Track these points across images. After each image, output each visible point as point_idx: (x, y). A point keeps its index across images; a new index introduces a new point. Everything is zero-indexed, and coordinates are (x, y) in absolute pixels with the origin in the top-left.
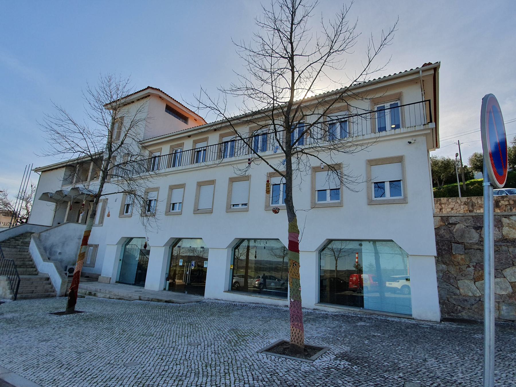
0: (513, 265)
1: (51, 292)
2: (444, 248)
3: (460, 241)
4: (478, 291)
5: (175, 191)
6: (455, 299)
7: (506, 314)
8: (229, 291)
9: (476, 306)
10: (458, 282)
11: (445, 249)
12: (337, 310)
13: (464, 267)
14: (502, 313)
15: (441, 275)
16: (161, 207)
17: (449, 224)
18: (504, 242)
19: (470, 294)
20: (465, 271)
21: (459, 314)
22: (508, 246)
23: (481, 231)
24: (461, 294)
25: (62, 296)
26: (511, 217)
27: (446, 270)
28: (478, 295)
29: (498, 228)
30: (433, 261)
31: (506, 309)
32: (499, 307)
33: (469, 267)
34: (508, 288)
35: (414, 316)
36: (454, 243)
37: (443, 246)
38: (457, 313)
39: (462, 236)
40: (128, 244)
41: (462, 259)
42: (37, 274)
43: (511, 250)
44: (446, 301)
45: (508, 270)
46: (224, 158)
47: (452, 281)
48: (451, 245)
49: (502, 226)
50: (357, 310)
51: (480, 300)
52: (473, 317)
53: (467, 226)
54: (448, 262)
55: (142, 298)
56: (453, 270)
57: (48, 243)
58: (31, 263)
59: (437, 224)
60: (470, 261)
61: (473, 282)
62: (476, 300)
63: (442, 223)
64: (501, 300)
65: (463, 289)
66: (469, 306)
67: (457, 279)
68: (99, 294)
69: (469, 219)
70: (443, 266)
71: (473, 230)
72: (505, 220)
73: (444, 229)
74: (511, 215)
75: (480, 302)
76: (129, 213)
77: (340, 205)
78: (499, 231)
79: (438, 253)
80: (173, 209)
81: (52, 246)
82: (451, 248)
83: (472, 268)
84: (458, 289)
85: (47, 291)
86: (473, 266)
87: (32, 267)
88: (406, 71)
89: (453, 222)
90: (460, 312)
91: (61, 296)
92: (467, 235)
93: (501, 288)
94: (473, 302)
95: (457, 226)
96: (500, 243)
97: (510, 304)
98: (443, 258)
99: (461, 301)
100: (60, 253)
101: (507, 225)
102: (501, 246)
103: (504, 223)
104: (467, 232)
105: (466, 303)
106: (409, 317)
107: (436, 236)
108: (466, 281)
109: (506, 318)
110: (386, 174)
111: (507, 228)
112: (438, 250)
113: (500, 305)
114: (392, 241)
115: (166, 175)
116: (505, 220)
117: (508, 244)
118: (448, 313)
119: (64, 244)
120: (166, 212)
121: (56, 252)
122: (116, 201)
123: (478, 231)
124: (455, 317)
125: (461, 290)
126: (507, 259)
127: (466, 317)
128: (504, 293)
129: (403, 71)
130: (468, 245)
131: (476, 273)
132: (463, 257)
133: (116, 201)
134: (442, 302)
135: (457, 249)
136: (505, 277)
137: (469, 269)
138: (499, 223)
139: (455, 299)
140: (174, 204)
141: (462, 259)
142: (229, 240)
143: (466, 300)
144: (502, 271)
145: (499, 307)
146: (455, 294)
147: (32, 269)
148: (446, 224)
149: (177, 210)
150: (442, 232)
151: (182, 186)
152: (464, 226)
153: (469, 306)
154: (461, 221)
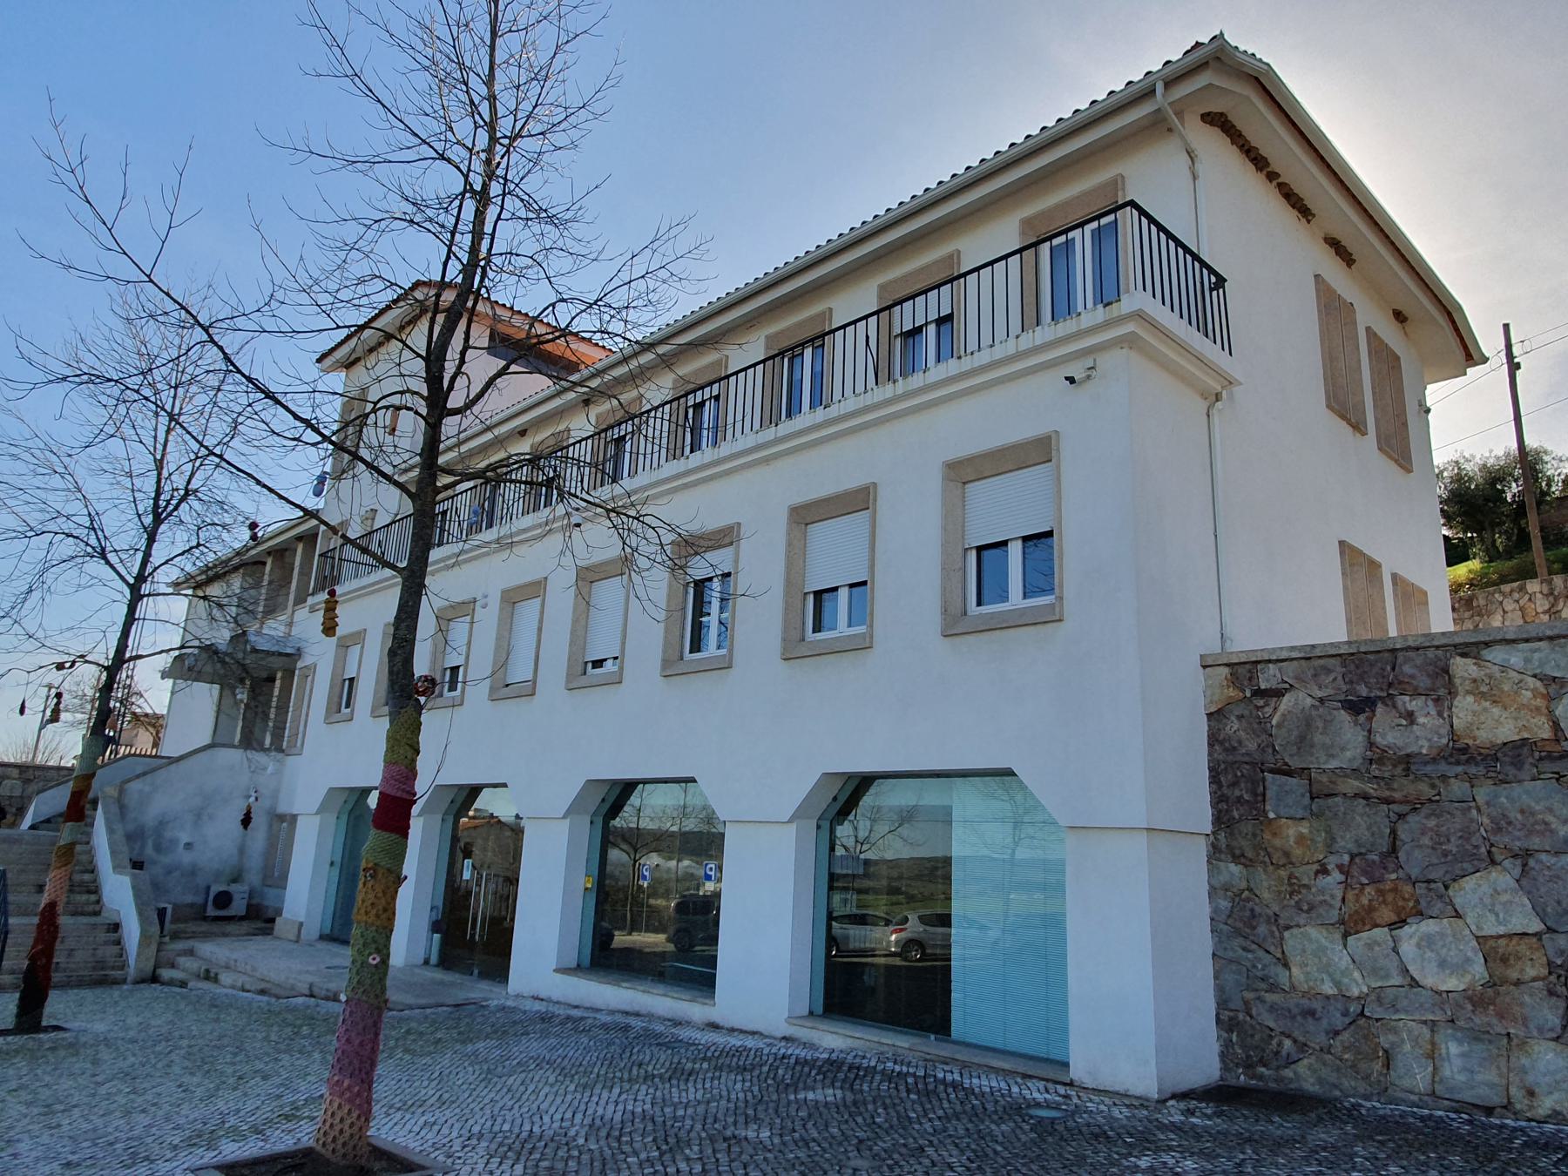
0: (1493, 862)
1: (113, 968)
2: (1237, 793)
3: (1295, 763)
4: (1356, 974)
5: (823, 534)
6: (1272, 1008)
7: (1461, 1078)
8: (578, 969)
9: (1345, 1036)
10: (1286, 934)
11: (1239, 799)
12: (850, 1043)
13: (1305, 873)
14: (1446, 1072)
15: (1224, 904)
16: (758, 616)
17: (1259, 693)
18: (1458, 763)
19: (1328, 989)
20: (1308, 887)
21: (1288, 1073)
22: (1471, 780)
23: (1370, 719)
24: (1293, 987)
25: (143, 981)
26: (1485, 653)
27: (1244, 885)
28: (1355, 992)
29: (1437, 700)
30: (1199, 851)
31: (1463, 1055)
32: (1433, 1044)
33: (1324, 871)
34: (1468, 960)
35: (1077, 1072)
36: (1272, 771)
37: (1234, 784)
38: (1278, 1068)
39: (1303, 742)
40: (615, 809)
41: (1301, 839)
42: (97, 914)
43: (1482, 794)
44: (1241, 1016)
45: (1469, 883)
46: (789, 415)
47: (1262, 929)
48: (1264, 780)
49: (1452, 693)
50: (930, 1046)
51: (1362, 1014)
52: (1335, 1086)
53: (1321, 700)
54: (1250, 854)
55: (316, 991)
56: (1266, 885)
57: (151, 815)
58: (87, 877)
59: (1216, 698)
60: (1331, 841)
61: (1338, 936)
62: (1345, 1014)
63: (1232, 692)
64: (1438, 1016)
65: (1304, 965)
66: (1321, 1039)
67: (1281, 922)
68: (226, 978)
69: (1328, 671)
70: (1232, 867)
71: (1344, 716)
72: (1462, 668)
73: (1240, 717)
74: (1487, 644)
75: (1362, 1022)
76: (711, 648)
77: (1051, 617)
78: (1440, 714)
79: (1218, 820)
80: (817, 628)
81: (162, 824)
82: (1264, 795)
83: (1338, 876)
84: (1286, 965)
85: (101, 964)
86: (1340, 867)
87: (89, 892)
88: (1168, 62)
89: (1273, 684)
90: (1290, 1062)
91: (137, 982)
92: (1318, 738)
93: (1442, 964)
94: (1339, 1021)
95: (1287, 702)
96: (1443, 767)
97: (1477, 1036)
98: (1232, 834)
99: (1293, 1017)
100: (188, 846)
101: (1468, 685)
102: (1444, 778)
103: (1457, 681)
104: (1320, 724)
105: (1310, 1024)
106: (1055, 1067)
107: (1211, 745)
108: (1313, 932)
109: (1457, 1097)
110: (1002, 510)
111: (1470, 699)
112: (1221, 803)
113: (1438, 1038)
114: (1009, 773)
115: (761, 458)
116: (1462, 668)
117: (1473, 770)
118: (1249, 1066)
119: (199, 816)
120: (666, 663)
121: (174, 842)
122: (22, 711)
123: (1362, 718)
124: (1272, 1085)
125: (1295, 970)
126: (1466, 835)
127: (1310, 1085)
128: (1453, 983)
129: (1101, 96)
130: (1324, 779)
131: (1350, 896)
132: (1304, 829)
133: (22, 711)
134: (1228, 1022)
135: (1283, 795)
136: (1458, 916)
137: (1324, 881)
138: (1439, 682)
139: (1272, 1008)
140: (818, 595)
141: (1301, 839)
142: (799, 782)
143: (1311, 1013)
144: (1446, 887)
145: (1433, 1044)
146: (1274, 988)
147: (84, 897)
148: (1248, 694)
149: (841, 626)
150: (1233, 726)
151: (859, 500)
152: (1309, 701)
153: (1321, 1039)
154: (1297, 678)
